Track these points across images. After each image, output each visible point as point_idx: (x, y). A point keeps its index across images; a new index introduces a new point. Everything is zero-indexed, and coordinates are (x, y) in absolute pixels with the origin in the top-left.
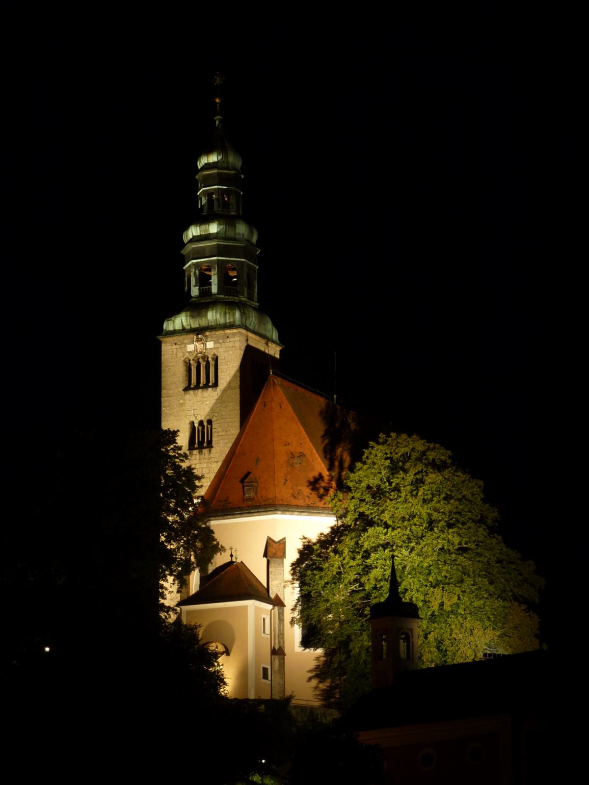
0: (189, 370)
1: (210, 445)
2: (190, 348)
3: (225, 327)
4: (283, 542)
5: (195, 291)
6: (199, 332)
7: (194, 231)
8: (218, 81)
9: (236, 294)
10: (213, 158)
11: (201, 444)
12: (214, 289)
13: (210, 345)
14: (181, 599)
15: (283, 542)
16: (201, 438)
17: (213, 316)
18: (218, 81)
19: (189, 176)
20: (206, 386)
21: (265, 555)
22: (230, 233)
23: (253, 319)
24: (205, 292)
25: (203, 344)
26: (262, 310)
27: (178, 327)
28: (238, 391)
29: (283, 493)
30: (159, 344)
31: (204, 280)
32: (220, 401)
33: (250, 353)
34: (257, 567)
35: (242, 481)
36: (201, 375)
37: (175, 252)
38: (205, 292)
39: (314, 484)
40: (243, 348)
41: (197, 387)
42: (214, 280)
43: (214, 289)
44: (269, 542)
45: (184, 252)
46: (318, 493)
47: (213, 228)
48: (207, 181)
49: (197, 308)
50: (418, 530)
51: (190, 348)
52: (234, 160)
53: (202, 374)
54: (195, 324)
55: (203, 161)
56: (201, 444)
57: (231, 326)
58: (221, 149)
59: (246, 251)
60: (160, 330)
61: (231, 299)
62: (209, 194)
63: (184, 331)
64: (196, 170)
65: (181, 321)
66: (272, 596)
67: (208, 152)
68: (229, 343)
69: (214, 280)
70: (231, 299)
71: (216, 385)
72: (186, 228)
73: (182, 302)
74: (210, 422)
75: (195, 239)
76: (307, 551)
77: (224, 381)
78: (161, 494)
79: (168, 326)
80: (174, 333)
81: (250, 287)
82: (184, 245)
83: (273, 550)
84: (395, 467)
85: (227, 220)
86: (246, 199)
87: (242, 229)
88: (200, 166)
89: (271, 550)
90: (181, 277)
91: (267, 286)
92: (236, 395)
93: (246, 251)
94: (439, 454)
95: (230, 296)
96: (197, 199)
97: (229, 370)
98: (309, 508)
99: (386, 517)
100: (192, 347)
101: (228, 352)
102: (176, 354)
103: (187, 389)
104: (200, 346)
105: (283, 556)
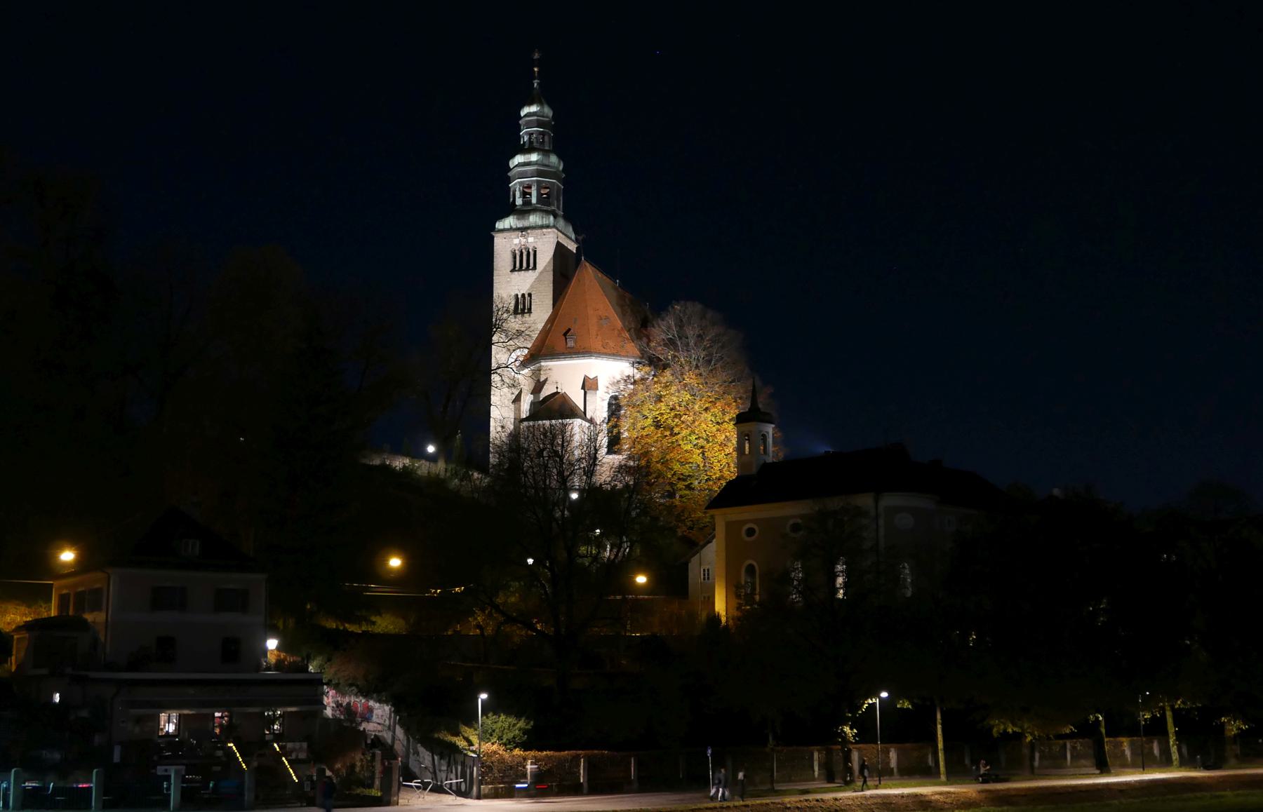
0: (515, 257)
1: (530, 311)
2: (516, 241)
3: (542, 227)
4: (596, 379)
5: (519, 201)
6: (523, 229)
7: (519, 159)
8: (536, 56)
9: (549, 205)
10: (534, 109)
11: (523, 310)
12: (534, 201)
13: (531, 239)
15: (596, 379)
16: (522, 306)
17: (534, 219)
18: (536, 56)
19: (514, 123)
20: (528, 269)
21: (583, 387)
22: (546, 162)
23: (561, 223)
24: (527, 203)
25: (257, 797)
26: (568, 218)
27: (507, 226)
28: (551, 273)
32: (538, 280)
33: (559, 246)
34: (577, 398)
35: (565, 335)
36: (523, 261)
38: (527, 203)
40: (553, 247)
41: (521, 269)
43: (534, 201)
44: (586, 380)
47: (534, 157)
48: (529, 125)
49: (523, 212)
51: (516, 241)
52: (548, 111)
53: (524, 254)
54: (520, 224)
55: (525, 111)
56: (523, 310)
57: (548, 227)
58: (540, 103)
60: (493, 229)
61: (545, 208)
62: (530, 134)
63: (511, 229)
64: (521, 118)
66: (588, 417)
67: (530, 104)
68: (546, 239)
69: (534, 193)
70: (545, 208)
71: (535, 268)
72: (513, 156)
73: (510, 210)
74: (530, 295)
75: (519, 165)
77: (540, 266)
78: (907, 705)
79: (500, 225)
81: (558, 201)
82: (521, 118)
83: (589, 385)
85: (546, 153)
86: (557, 137)
87: (554, 159)
88: (522, 114)
91: (572, 201)
95: (545, 205)
96: (519, 137)
97: (545, 258)
100: (517, 241)
102: (505, 245)
103: (513, 270)
104: (523, 240)
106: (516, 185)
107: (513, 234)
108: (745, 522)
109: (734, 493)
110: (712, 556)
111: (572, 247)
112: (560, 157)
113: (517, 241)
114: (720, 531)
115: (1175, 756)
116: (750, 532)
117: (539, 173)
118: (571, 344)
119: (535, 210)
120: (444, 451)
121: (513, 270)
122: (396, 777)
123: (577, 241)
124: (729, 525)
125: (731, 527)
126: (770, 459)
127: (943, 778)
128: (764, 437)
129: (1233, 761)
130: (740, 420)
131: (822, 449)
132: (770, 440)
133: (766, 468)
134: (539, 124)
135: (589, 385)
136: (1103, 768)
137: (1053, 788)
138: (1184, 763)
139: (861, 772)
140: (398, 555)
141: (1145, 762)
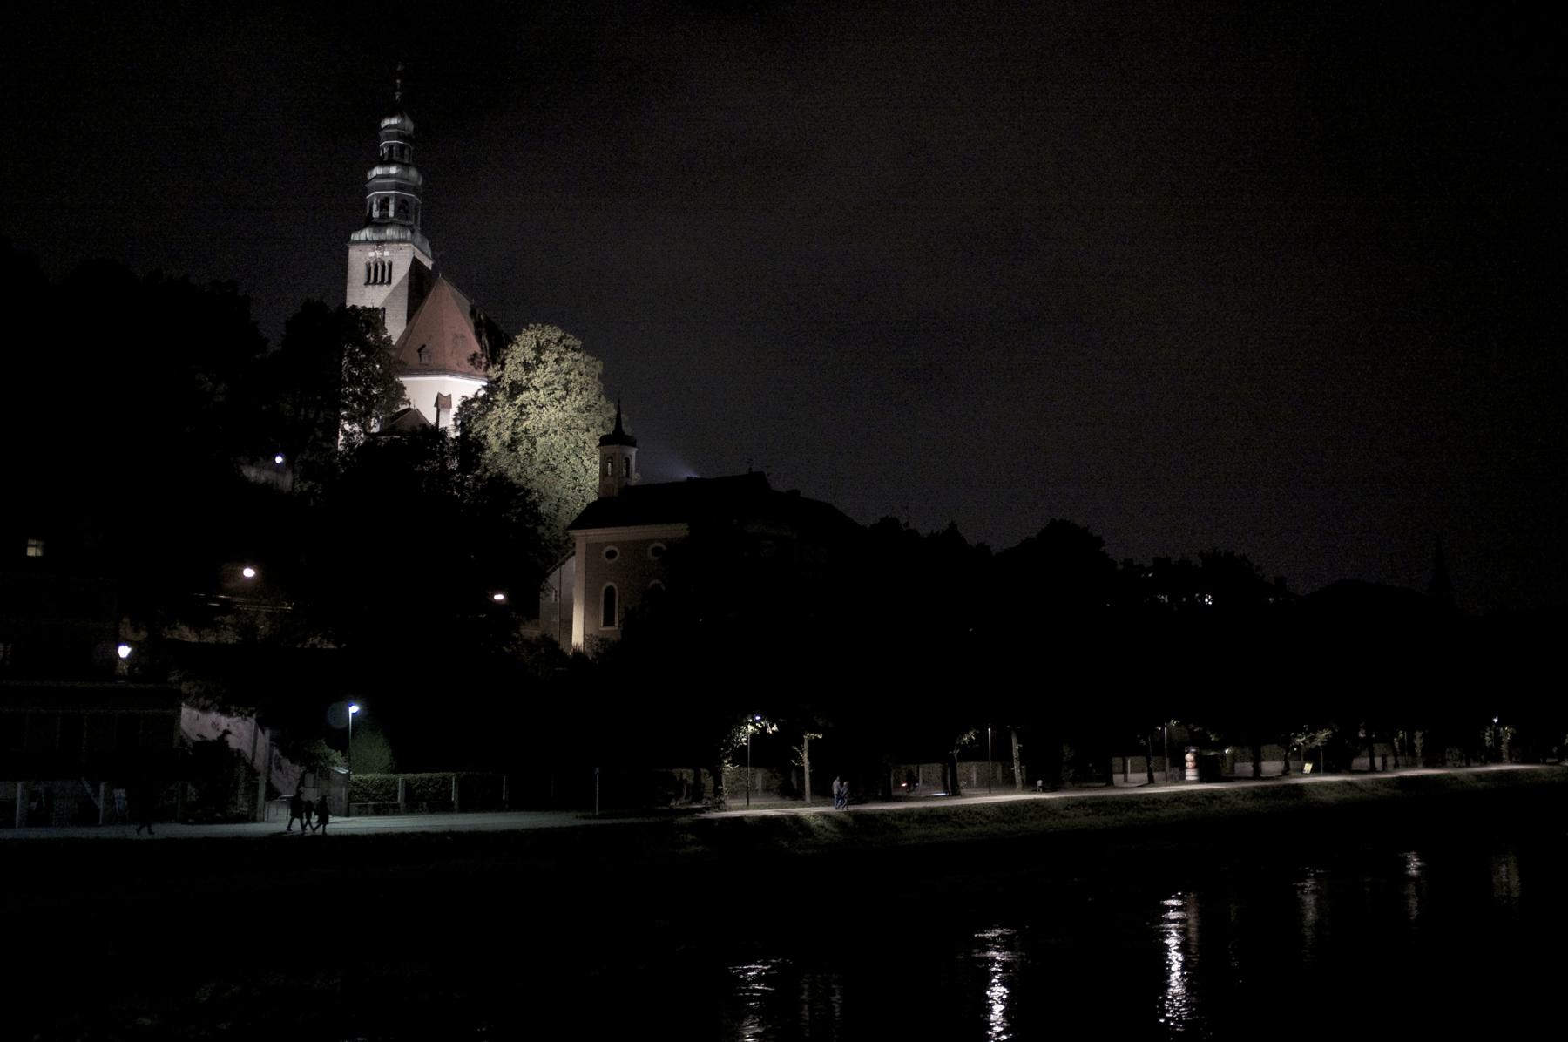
2: (371, 254)
3: (399, 241)
4: (449, 397)
5: (376, 214)
6: (379, 243)
7: (378, 171)
10: (395, 121)
12: (391, 214)
13: (387, 253)
14: (603, 485)
15: (449, 397)
17: (390, 233)
20: (382, 282)
21: (436, 404)
23: (418, 238)
24: (384, 216)
29: (451, 362)
30: (348, 249)
31: (384, 205)
32: (393, 294)
33: (415, 262)
36: (378, 274)
37: (362, 186)
38: (384, 216)
39: (473, 359)
41: (375, 282)
42: (392, 207)
43: (391, 214)
44: (439, 397)
45: (368, 186)
46: (473, 365)
47: (393, 170)
48: (388, 137)
49: (380, 225)
50: (558, 394)
51: (371, 254)
52: (409, 125)
54: (376, 237)
55: (387, 122)
57: (404, 241)
58: (402, 116)
59: (415, 190)
62: (391, 147)
63: (367, 241)
65: (366, 234)
67: (391, 116)
68: (401, 253)
71: (390, 282)
73: (368, 222)
75: (378, 177)
76: (466, 403)
79: (355, 237)
80: (359, 242)
83: (441, 403)
84: (539, 349)
87: (413, 173)
89: (441, 402)
90: (363, 204)
91: (423, 214)
92: (405, 291)
93: (415, 190)
94: (572, 341)
97: (401, 272)
98: (469, 375)
99: (536, 382)
100: (372, 254)
101: (401, 258)
102: (360, 257)
103: (367, 283)
104: (379, 254)
105: (450, 406)
106: (374, 196)
107: (369, 247)
108: (652, 541)
109: (593, 516)
110: (571, 577)
111: (428, 263)
112: (420, 171)
113: (372, 254)
114: (580, 549)
115: (1018, 778)
116: (611, 555)
117: (399, 187)
118: (425, 360)
119: (391, 224)
120: (289, 461)
121: (367, 283)
122: (262, 792)
123: (434, 258)
124: (589, 546)
125: (592, 548)
126: (633, 483)
127: (808, 799)
128: (628, 461)
129: (1069, 784)
130: (604, 441)
131: (684, 473)
132: (633, 462)
133: (627, 491)
134: (400, 137)
135: (441, 403)
136: (955, 793)
137: (932, 810)
138: (1029, 785)
139: (1018, 821)
140: (251, 566)
141: (989, 785)
